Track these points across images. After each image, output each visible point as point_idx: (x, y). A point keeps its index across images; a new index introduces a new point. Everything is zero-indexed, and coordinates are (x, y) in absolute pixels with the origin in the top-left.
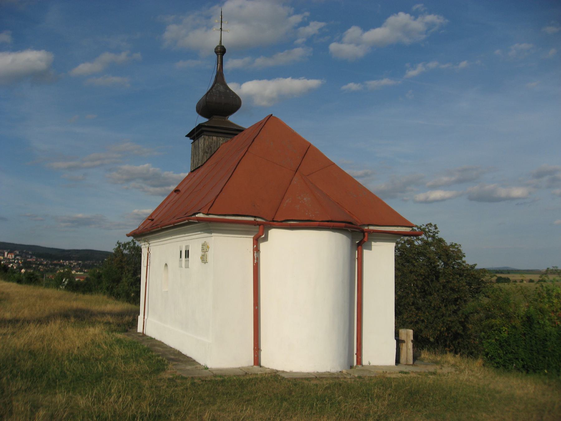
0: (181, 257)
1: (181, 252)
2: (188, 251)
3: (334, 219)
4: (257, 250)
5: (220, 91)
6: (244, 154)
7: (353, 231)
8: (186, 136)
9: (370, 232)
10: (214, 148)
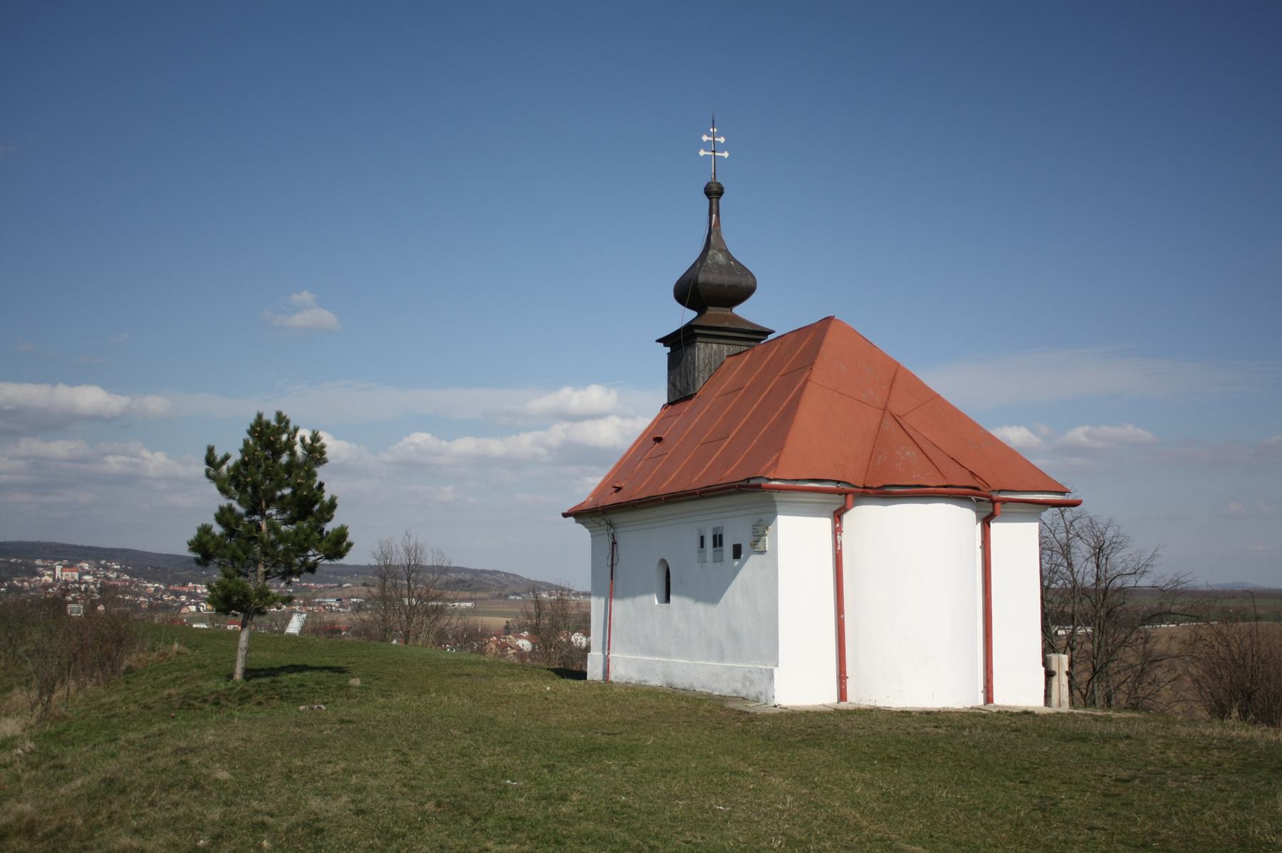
0: (702, 546)
1: (702, 538)
2: (721, 536)
3: (956, 484)
4: (837, 531)
5: (720, 263)
6: (904, 430)
7: (978, 500)
8: (659, 341)
9: (1004, 502)
10: (715, 362)
